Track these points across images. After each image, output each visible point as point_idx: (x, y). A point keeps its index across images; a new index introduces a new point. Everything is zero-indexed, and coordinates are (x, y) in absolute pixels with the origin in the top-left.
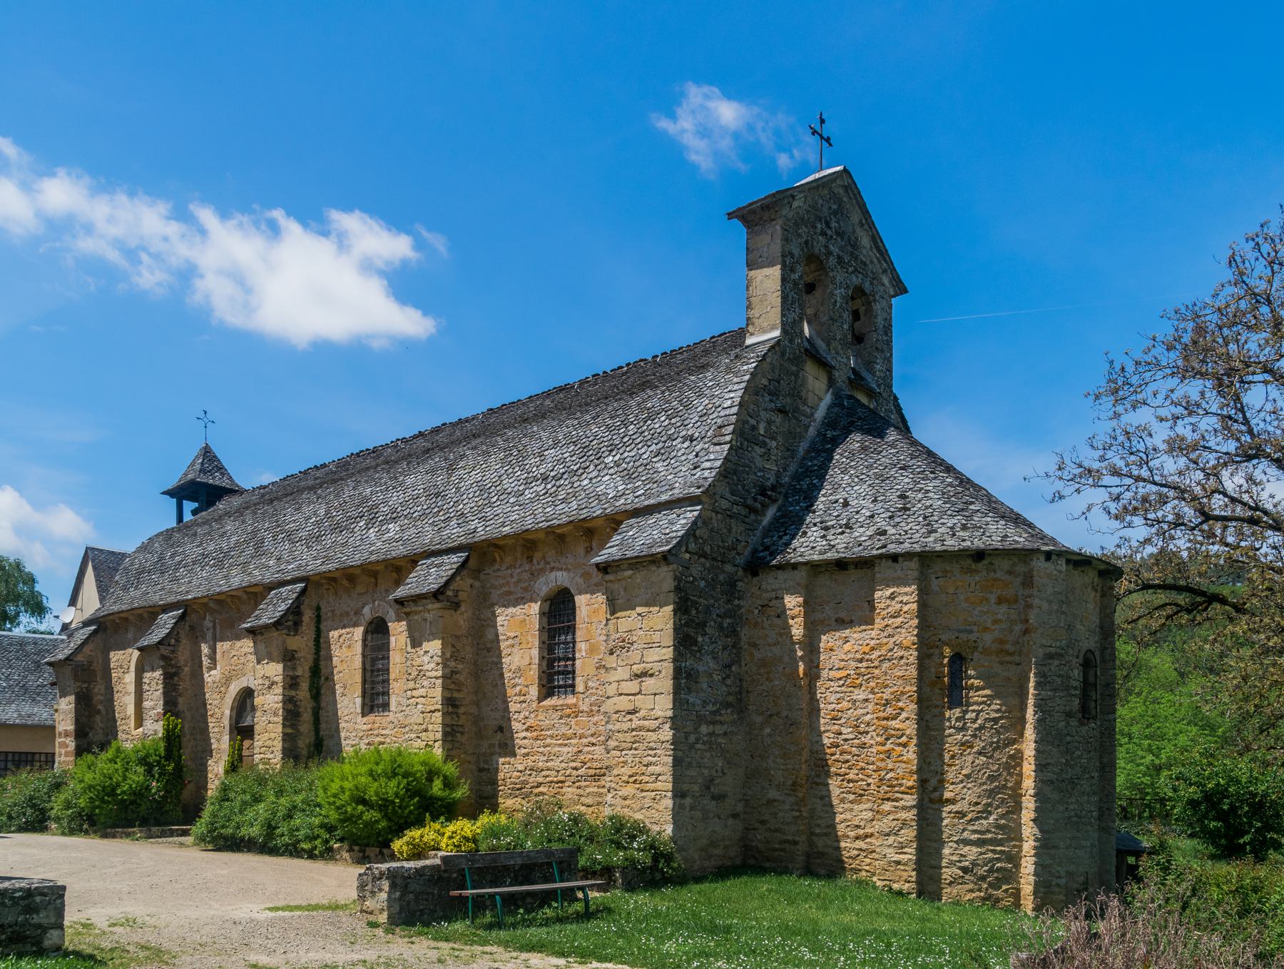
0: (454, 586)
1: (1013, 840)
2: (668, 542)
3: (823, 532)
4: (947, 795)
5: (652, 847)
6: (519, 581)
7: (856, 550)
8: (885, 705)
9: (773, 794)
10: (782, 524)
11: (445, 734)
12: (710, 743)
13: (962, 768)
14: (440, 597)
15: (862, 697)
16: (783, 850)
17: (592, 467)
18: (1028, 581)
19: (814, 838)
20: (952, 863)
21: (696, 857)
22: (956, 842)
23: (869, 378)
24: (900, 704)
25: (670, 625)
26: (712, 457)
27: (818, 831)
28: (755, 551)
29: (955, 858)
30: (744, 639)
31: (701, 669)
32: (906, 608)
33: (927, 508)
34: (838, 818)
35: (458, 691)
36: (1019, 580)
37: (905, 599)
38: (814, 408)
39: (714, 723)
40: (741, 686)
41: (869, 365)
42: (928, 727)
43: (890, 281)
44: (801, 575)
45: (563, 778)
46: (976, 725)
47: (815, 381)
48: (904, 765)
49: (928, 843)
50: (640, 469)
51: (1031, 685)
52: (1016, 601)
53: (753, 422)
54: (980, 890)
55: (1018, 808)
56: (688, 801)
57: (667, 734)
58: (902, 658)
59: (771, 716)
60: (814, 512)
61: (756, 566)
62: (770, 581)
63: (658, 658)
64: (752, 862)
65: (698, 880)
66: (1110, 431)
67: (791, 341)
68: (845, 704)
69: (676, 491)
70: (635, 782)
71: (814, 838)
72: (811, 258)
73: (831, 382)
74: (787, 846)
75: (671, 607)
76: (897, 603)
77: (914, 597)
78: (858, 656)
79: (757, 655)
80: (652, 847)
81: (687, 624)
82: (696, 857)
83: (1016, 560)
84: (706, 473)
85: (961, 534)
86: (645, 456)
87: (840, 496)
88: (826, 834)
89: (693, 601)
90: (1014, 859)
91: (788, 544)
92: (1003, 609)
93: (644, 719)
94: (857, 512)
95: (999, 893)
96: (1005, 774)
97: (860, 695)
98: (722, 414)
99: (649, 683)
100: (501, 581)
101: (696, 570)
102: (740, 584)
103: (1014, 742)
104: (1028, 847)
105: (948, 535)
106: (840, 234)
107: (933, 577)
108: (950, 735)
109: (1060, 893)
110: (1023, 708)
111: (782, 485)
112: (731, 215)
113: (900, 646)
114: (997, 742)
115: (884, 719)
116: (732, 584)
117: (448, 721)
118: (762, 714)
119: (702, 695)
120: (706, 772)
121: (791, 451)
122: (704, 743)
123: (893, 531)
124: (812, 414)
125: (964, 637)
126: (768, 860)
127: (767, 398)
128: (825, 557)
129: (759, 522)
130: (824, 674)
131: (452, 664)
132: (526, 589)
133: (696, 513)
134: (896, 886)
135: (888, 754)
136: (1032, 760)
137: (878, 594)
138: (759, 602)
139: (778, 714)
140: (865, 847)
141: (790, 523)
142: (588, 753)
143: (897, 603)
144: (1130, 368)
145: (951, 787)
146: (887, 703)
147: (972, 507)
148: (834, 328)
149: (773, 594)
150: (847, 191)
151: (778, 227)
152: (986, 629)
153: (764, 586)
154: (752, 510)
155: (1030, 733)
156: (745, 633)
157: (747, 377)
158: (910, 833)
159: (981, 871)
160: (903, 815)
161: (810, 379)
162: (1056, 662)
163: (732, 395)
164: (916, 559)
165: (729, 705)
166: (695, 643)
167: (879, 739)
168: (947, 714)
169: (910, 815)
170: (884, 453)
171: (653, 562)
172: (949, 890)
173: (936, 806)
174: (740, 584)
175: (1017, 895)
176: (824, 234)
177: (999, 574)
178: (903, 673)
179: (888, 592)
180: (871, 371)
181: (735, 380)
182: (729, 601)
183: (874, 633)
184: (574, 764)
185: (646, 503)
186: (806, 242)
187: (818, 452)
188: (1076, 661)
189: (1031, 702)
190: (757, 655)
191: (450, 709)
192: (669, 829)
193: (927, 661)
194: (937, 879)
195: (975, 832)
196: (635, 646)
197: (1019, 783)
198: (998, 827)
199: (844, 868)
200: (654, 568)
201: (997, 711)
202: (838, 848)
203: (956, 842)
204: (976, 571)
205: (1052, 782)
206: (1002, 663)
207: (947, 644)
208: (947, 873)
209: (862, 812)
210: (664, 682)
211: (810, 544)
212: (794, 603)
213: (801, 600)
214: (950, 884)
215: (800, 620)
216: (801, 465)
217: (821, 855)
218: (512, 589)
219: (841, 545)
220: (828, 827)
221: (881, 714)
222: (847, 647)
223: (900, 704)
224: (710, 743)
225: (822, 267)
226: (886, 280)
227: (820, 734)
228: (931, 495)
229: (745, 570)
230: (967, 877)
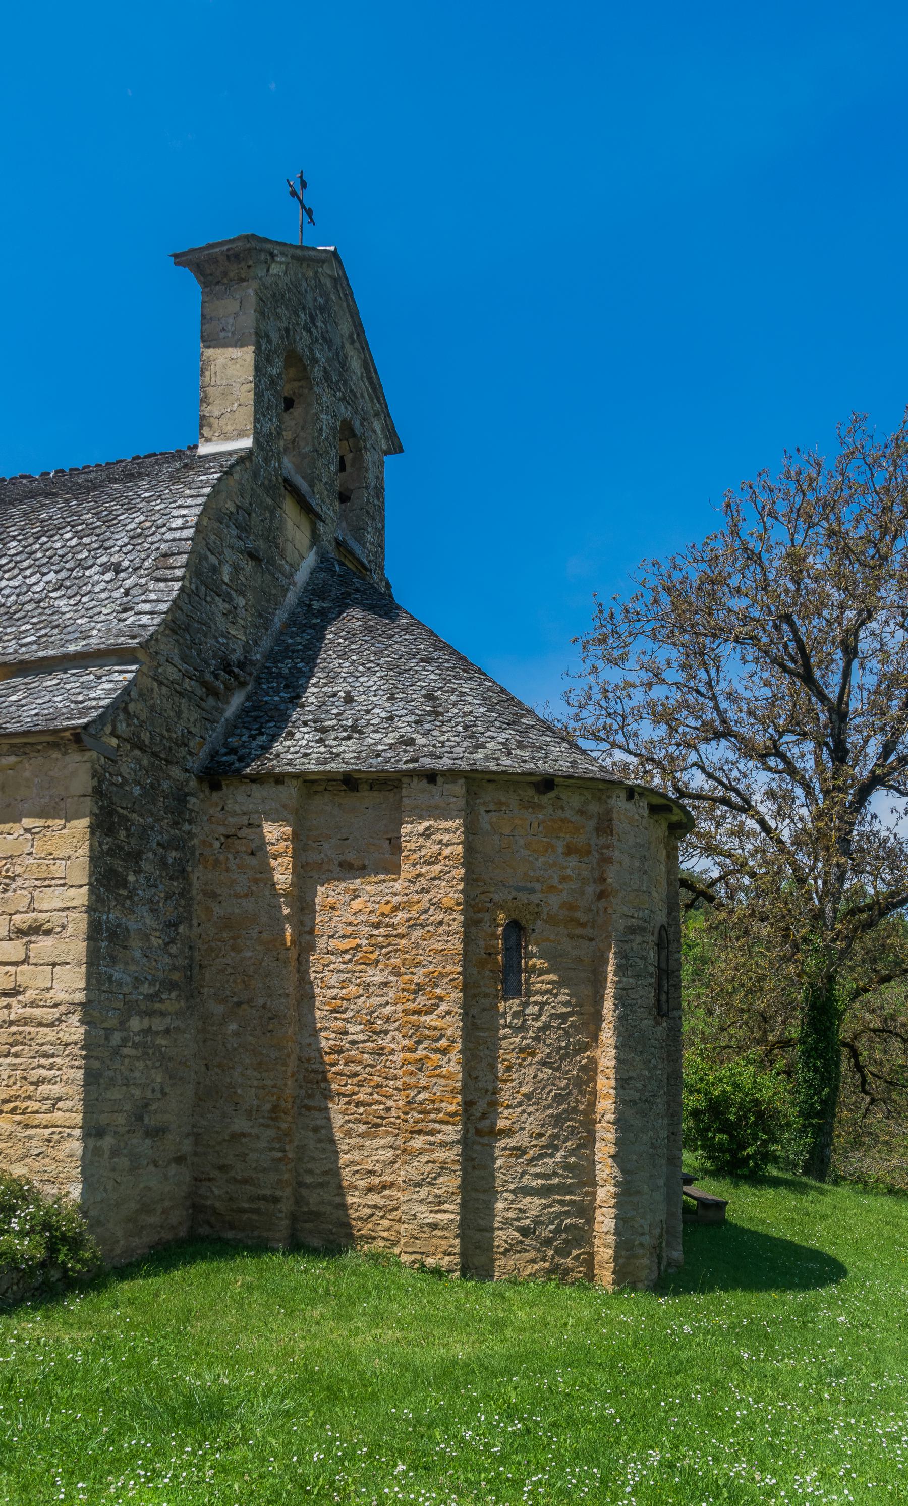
1: (585, 1184)
2: (82, 714)
4: (502, 1124)
5: (47, 1226)
7: (373, 761)
8: (416, 992)
9: (240, 1124)
10: (256, 719)
13: (520, 1084)
15: (378, 979)
16: (256, 1211)
18: (605, 826)
19: (304, 1192)
20: (507, 1223)
21: (120, 1233)
22: (513, 1192)
23: (357, 549)
24: (438, 991)
25: (84, 851)
26: (153, 597)
27: (308, 1179)
28: (213, 755)
29: (511, 1215)
30: (196, 884)
31: (132, 926)
32: (447, 851)
33: (466, 714)
34: (344, 1159)
36: (592, 824)
37: (446, 838)
38: (294, 567)
39: (150, 1014)
40: (191, 958)
41: (358, 532)
43: (383, 430)
44: (290, 793)
46: (539, 1024)
47: (295, 531)
48: (443, 1081)
49: (474, 1195)
50: (28, 607)
51: (611, 968)
52: (589, 852)
53: (213, 560)
54: (544, 1260)
55: (590, 1139)
56: (108, 1142)
57: (74, 1030)
58: (441, 923)
59: (239, 1004)
60: (303, 706)
61: (216, 775)
62: (239, 799)
64: (204, 1230)
65: (124, 1272)
66: (586, 688)
67: (267, 460)
68: (352, 989)
69: (94, 641)
70: (13, 1111)
71: (304, 1192)
72: (293, 359)
73: (315, 538)
74: (262, 1205)
75: (85, 822)
76: (434, 843)
77: (459, 836)
78: (374, 919)
79: (218, 911)
80: (47, 1226)
81: (110, 852)
82: (120, 1233)
83: (589, 796)
84: (145, 619)
85: (518, 752)
86: (37, 588)
87: (341, 688)
88: (321, 1185)
89: (121, 816)
90: (586, 1211)
91: (266, 748)
92: (573, 862)
93: (33, 1004)
94: (368, 712)
95: (568, 1262)
96: (575, 1092)
97: (375, 976)
98: (169, 536)
99: (43, 945)
101: (126, 767)
102: (193, 800)
103: (585, 1047)
104: (605, 1193)
105: (496, 752)
107: (482, 810)
108: (505, 1038)
109: (643, 1256)
110: (598, 1000)
111: (253, 664)
112: (180, 259)
113: (439, 905)
114: (566, 1048)
115: (415, 1012)
116: (181, 797)
118: (224, 1001)
119: (133, 968)
120: (137, 1092)
121: (263, 619)
122: (135, 1046)
123: (424, 741)
125: (523, 897)
126: (232, 1227)
127: (234, 532)
128: (328, 767)
129: (222, 712)
130: (321, 943)
133: (129, 676)
134: (430, 1261)
135: (420, 1064)
136: (611, 1073)
137: (406, 829)
138: (222, 830)
139: (250, 1001)
140: (381, 1202)
141: (269, 717)
143: (434, 843)
144: (619, 616)
145: (506, 1113)
146: (419, 989)
147: (524, 721)
149: (245, 820)
150: (336, 287)
151: (251, 292)
152: (552, 888)
154: (212, 692)
155: (608, 1035)
156: (198, 876)
157: (207, 490)
158: (450, 1182)
159: (546, 1232)
160: (443, 1155)
161: (289, 524)
162: (639, 939)
163: (184, 512)
164: (462, 781)
165: (173, 986)
166: (124, 884)
167: (406, 1042)
168: (501, 1007)
169: (451, 1155)
170: (396, 638)
171: (55, 745)
172: (503, 1263)
173: (485, 1140)
174: (193, 800)
175: (589, 1262)
177: (568, 814)
178: (442, 945)
179: (421, 827)
180: (360, 540)
181: (188, 492)
182: (176, 824)
183: (398, 886)
185: (41, 654)
187: (303, 627)
188: (652, 939)
189: (610, 991)
190: (218, 911)
192: (75, 1191)
193: (474, 930)
194: (486, 1247)
195: (538, 1176)
196: (19, 882)
197: (592, 1105)
198: (567, 1167)
199: (351, 1236)
200: (56, 755)
201: (566, 1004)
202: (343, 1207)
203: (513, 1192)
204: (541, 807)
205: (635, 1103)
206: (571, 937)
207: (501, 907)
208: (502, 1237)
209: (378, 1150)
210: (73, 945)
211: (299, 748)
212: (277, 834)
213: (288, 830)
214: (504, 1253)
215: (287, 860)
216: (278, 641)
217: (316, 1216)
219: (348, 754)
220: (326, 1173)
221: (410, 1006)
222: (356, 904)
223: (438, 991)
225: (304, 376)
226: (377, 426)
227: (315, 1033)
228: (469, 698)
229: (200, 779)
230: (527, 1241)
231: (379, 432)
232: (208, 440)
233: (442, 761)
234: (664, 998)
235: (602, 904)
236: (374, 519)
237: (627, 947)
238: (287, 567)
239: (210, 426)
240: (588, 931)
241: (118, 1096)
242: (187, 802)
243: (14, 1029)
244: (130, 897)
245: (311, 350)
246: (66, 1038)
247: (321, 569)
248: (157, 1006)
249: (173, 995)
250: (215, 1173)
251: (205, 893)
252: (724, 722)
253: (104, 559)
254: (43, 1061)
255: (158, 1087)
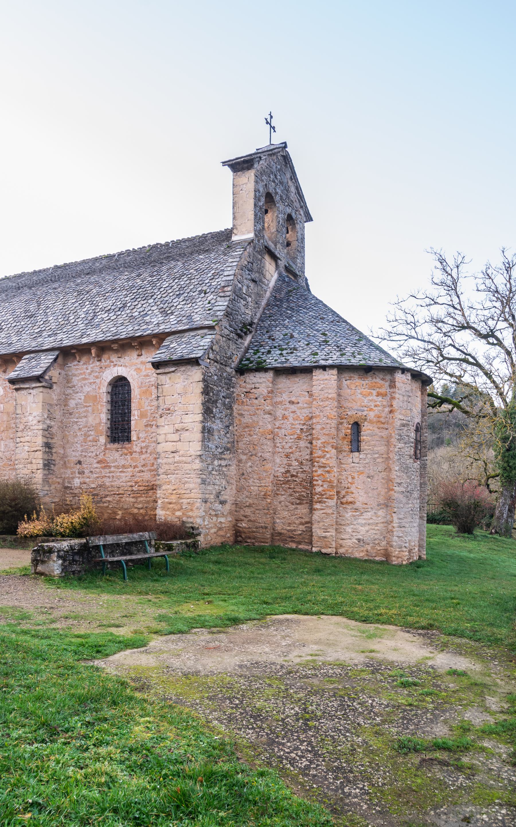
0: (50, 373)
3: (280, 352)
6: (92, 371)
11: (45, 465)
12: (219, 471)
14: (41, 379)
17: (140, 305)
31: (215, 427)
35: (52, 438)
41: (294, 259)
42: (341, 463)
43: (304, 214)
45: (122, 492)
47: (269, 266)
59: (251, 455)
63: (191, 420)
67: (259, 241)
81: (208, 401)
85: (358, 356)
89: (211, 388)
92: (380, 398)
93: (183, 456)
98: (223, 279)
99: (186, 435)
100: (79, 372)
101: (212, 370)
106: (281, 183)
112: (224, 163)
117: (46, 457)
118: (246, 454)
122: (216, 471)
124: (268, 284)
125: (360, 413)
127: (247, 272)
131: (48, 422)
132: (97, 377)
138: (245, 390)
139: (255, 455)
142: (140, 477)
148: (278, 236)
151: (253, 174)
153: (247, 381)
154: (240, 336)
161: (267, 264)
162: (406, 429)
166: (212, 412)
176: (274, 182)
184: (130, 484)
186: (266, 185)
188: (413, 428)
191: (47, 450)
193: (340, 426)
205: (403, 492)
210: (196, 434)
218: (87, 377)
224: (219, 471)
229: (236, 371)
231: (302, 214)
232: (236, 235)
233: (328, 362)
234: (418, 452)
235: (391, 415)
236: (300, 252)
237: (401, 432)
238: (266, 282)
239: (237, 229)
240: (386, 426)
241: (211, 488)
242: (231, 380)
243: (176, 465)
244: (214, 417)
245: (275, 189)
246: (195, 468)
247: (280, 280)
248: (223, 456)
249: (228, 452)
250: (243, 518)
251: (239, 414)
252: (468, 323)
253: (200, 289)
254: (187, 476)
255: (223, 486)
